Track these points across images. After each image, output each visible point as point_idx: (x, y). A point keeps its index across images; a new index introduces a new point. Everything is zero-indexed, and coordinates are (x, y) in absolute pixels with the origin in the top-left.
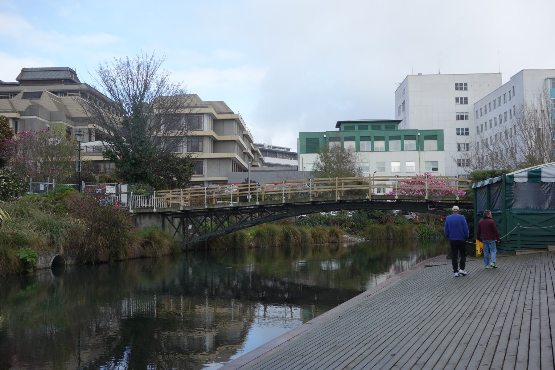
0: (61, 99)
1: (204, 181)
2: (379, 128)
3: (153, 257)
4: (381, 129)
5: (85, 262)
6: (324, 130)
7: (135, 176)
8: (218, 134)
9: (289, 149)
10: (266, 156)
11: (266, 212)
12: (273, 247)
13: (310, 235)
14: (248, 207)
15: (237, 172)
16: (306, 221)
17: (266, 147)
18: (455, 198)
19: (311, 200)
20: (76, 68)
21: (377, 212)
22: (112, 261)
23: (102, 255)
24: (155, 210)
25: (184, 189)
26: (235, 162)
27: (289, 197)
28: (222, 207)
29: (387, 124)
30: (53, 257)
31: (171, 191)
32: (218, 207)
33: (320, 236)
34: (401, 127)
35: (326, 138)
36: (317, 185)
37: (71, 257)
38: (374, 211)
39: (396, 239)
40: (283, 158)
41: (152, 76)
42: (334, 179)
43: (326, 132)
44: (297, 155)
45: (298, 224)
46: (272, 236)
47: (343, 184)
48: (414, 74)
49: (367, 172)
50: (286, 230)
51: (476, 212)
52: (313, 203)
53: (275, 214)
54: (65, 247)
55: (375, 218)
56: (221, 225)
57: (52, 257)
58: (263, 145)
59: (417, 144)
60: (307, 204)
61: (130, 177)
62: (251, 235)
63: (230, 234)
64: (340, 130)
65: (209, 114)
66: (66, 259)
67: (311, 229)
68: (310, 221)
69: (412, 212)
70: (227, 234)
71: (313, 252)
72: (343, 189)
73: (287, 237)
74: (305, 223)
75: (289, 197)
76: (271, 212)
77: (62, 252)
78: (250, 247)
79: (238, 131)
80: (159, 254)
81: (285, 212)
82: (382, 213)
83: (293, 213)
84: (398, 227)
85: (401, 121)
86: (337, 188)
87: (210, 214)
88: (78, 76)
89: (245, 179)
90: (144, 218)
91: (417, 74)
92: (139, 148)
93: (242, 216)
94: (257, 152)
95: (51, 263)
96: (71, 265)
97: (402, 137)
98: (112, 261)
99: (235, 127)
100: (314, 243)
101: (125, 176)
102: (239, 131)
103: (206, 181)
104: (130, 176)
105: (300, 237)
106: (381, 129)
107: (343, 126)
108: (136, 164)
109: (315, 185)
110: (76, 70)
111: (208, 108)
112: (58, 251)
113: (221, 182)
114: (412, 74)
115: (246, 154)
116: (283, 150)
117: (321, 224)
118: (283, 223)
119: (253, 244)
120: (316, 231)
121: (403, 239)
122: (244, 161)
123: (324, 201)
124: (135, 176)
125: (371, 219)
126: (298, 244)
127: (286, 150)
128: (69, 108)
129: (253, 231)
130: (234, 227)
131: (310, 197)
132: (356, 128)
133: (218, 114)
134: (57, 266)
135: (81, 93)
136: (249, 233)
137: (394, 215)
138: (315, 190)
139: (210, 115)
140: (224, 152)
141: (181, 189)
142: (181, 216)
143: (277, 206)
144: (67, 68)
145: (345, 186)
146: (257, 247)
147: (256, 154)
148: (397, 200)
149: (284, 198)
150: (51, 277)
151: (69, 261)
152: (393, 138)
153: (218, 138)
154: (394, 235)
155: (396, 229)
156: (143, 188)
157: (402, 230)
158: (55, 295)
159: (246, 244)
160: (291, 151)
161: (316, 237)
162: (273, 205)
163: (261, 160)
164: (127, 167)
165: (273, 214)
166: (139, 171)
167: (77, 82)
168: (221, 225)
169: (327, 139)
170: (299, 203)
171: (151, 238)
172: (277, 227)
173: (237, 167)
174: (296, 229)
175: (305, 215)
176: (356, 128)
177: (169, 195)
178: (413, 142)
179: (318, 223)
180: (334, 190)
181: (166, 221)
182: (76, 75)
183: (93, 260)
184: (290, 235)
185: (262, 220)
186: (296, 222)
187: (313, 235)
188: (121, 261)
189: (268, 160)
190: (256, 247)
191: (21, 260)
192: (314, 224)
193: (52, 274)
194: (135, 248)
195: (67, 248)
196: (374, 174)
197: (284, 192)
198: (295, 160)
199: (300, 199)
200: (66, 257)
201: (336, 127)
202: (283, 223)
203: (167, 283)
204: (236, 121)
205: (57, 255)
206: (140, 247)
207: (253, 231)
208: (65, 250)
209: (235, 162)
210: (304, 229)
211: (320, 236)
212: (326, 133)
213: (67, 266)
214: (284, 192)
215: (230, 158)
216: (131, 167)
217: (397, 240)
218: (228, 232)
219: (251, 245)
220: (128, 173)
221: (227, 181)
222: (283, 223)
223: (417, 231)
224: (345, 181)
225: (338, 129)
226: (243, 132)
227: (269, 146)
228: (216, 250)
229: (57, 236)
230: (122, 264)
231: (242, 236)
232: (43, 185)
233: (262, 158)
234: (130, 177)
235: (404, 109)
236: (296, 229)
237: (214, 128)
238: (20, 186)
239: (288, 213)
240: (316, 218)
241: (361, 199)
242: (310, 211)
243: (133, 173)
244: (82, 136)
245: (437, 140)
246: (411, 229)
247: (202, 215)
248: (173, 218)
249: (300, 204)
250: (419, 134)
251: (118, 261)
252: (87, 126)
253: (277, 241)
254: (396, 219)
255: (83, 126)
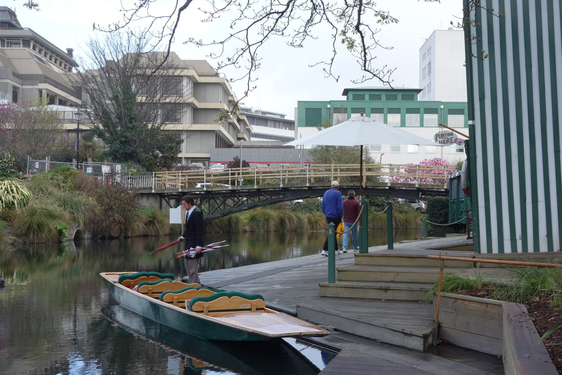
0: (4, 51)
1: (182, 158)
2: (395, 98)
3: (155, 236)
4: (396, 100)
5: (100, 236)
6: (328, 100)
7: (124, 155)
8: (199, 101)
9: (283, 116)
10: (254, 125)
11: (263, 196)
12: (268, 232)
13: (306, 221)
14: (293, 188)
15: (222, 148)
16: (303, 207)
17: (253, 113)
18: (443, 186)
19: (308, 185)
20: (15, 8)
21: (380, 199)
22: (122, 237)
23: (115, 232)
24: (153, 191)
25: (183, 171)
26: (219, 135)
27: (286, 182)
28: (220, 190)
29: (405, 93)
30: (75, 231)
31: (167, 172)
32: (216, 189)
33: (316, 222)
34: (420, 97)
35: (329, 108)
36: (314, 170)
37: (88, 231)
38: (377, 198)
39: (399, 229)
40: (275, 127)
41: (156, 58)
42: (330, 165)
43: (330, 102)
44: (294, 124)
45: (294, 210)
46: (267, 220)
47: (339, 170)
48: (442, 29)
49: (378, 152)
50: (282, 215)
51: (451, 200)
52: (310, 188)
53: (271, 198)
54: (84, 223)
55: (378, 206)
56: (218, 208)
57: (74, 231)
58: (250, 110)
59: (439, 119)
60: (304, 188)
61: (120, 156)
62: (246, 219)
63: (225, 217)
64: (348, 99)
65: (189, 77)
66: (84, 234)
67: (308, 214)
68: (307, 207)
69: (420, 201)
70: (223, 216)
71: (309, 239)
72: (339, 175)
73: (282, 222)
74: (302, 209)
75: (286, 182)
76: (268, 196)
77: (82, 227)
78: (245, 232)
79: (224, 96)
80: (161, 233)
81: (282, 196)
82: (385, 200)
83: (290, 198)
84: (402, 216)
85: (422, 90)
86: (332, 174)
87: (208, 196)
88: (18, 18)
89: (234, 158)
90: (142, 198)
91: (447, 29)
92: (129, 125)
93: (238, 199)
94: (243, 121)
95: (73, 236)
96: (88, 239)
97: (422, 110)
98: (122, 237)
99: (220, 93)
100: (311, 229)
101: (114, 154)
102: (224, 95)
103: (184, 158)
104: (120, 154)
105: (296, 223)
106: (396, 100)
107: (350, 94)
108: (125, 142)
109: (312, 171)
110: (15, 10)
111: (188, 69)
112: (79, 225)
113: (201, 160)
114: (440, 29)
115: (231, 124)
116: (276, 117)
117: (318, 210)
118: (278, 208)
119: (247, 228)
120: (312, 218)
121: (407, 229)
122: (229, 133)
123: (320, 187)
124: (124, 155)
125: (373, 207)
126: (294, 230)
127: (279, 117)
128: (15, 63)
129: (248, 215)
130: (231, 210)
131: (306, 182)
132: (367, 97)
133: (200, 76)
134: (78, 239)
135: (23, 40)
136: (244, 217)
137: (398, 202)
138: (312, 175)
139: (190, 78)
140: (206, 124)
141: (180, 171)
142: (176, 197)
143: (274, 190)
144: (6, 7)
145: (341, 173)
146: (252, 232)
147: (242, 123)
148: (389, 187)
149: (281, 182)
150: (73, 249)
151: (87, 236)
152: (410, 111)
153: (199, 105)
154: (396, 224)
155: (400, 217)
156: (134, 168)
157: (405, 219)
158: (75, 264)
159: (241, 228)
160: (286, 118)
161: (312, 223)
162: (270, 189)
163: (249, 130)
164: (117, 145)
165: (269, 198)
166: (129, 150)
167: (17, 25)
168: (218, 208)
169: (332, 111)
170: (296, 187)
171: (154, 218)
172: (273, 213)
173: (222, 142)
174: (292, 214)
175: (300, 201)
176: (367, 97)
177: (169, 177)
178: (435, 117)
179: (315, 210)
180: (330, 175)
181: (164, 202)
182: (15, 16)
183: (106, 236)
184: (286, 221)
185: (259, 203)
186: (291, 208)
187: (310, 221)
188: (129, 237)
189: (256, 129)
190: (250, 232)
191: (58, 230)
192: (311, 210)
193: (74, 245)
194: (139, 227)
195: (86, 223)
196: (381, 157)
197: (281, 177)
198: (291, 129)
199: (297, 184)
200: (85, 231)
201: (344, 94)
202: (278, 208)
203: (163, 264)
204: (221, 86)
205: (78, 229)
206: (144, 226)
207: (248, 215)
208: (84, 225)
209: (219, 135)
210: (300, 215)
211: (316, 222)
212: (330, 102)
213: (84, 240)
214: (281, 177)
215: (214, 131)
216: (121, 145)
217: (400, 230)
218: (224, 215)
219: (246, 229)
220: (118, 151)
221: (209, 158)
222: (279, 208)
223: (422, 221)
224: (341, 168)
225: (345, 98)
226: (228, 98)
227: (256, 111)
228: (211, 232)
229: (77, 212)
230: (129, 240)
231: (238, 220)
232: (38, 163)
233: (250, 129)
234: (120, 156)
235: (430, 72)
236: (292, 214)
237: (195, 94)
238: (5, 162)
239: (285, 197)
240: (314, 204)
241: (356, 185)
242: (307, 195)
243: (122, 151)
244: (81, 115)
245: (464, 114)
246: (416, 218)
247: (198, 197)
248: (169, 199)
249: (297, 189)
250: (442, 107)
251: (126, 237)
252: (37, 85)
253: (272, 226)
254: (400, 207)
255: (33, 85)
